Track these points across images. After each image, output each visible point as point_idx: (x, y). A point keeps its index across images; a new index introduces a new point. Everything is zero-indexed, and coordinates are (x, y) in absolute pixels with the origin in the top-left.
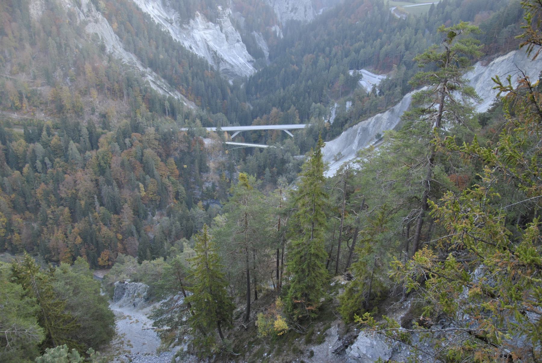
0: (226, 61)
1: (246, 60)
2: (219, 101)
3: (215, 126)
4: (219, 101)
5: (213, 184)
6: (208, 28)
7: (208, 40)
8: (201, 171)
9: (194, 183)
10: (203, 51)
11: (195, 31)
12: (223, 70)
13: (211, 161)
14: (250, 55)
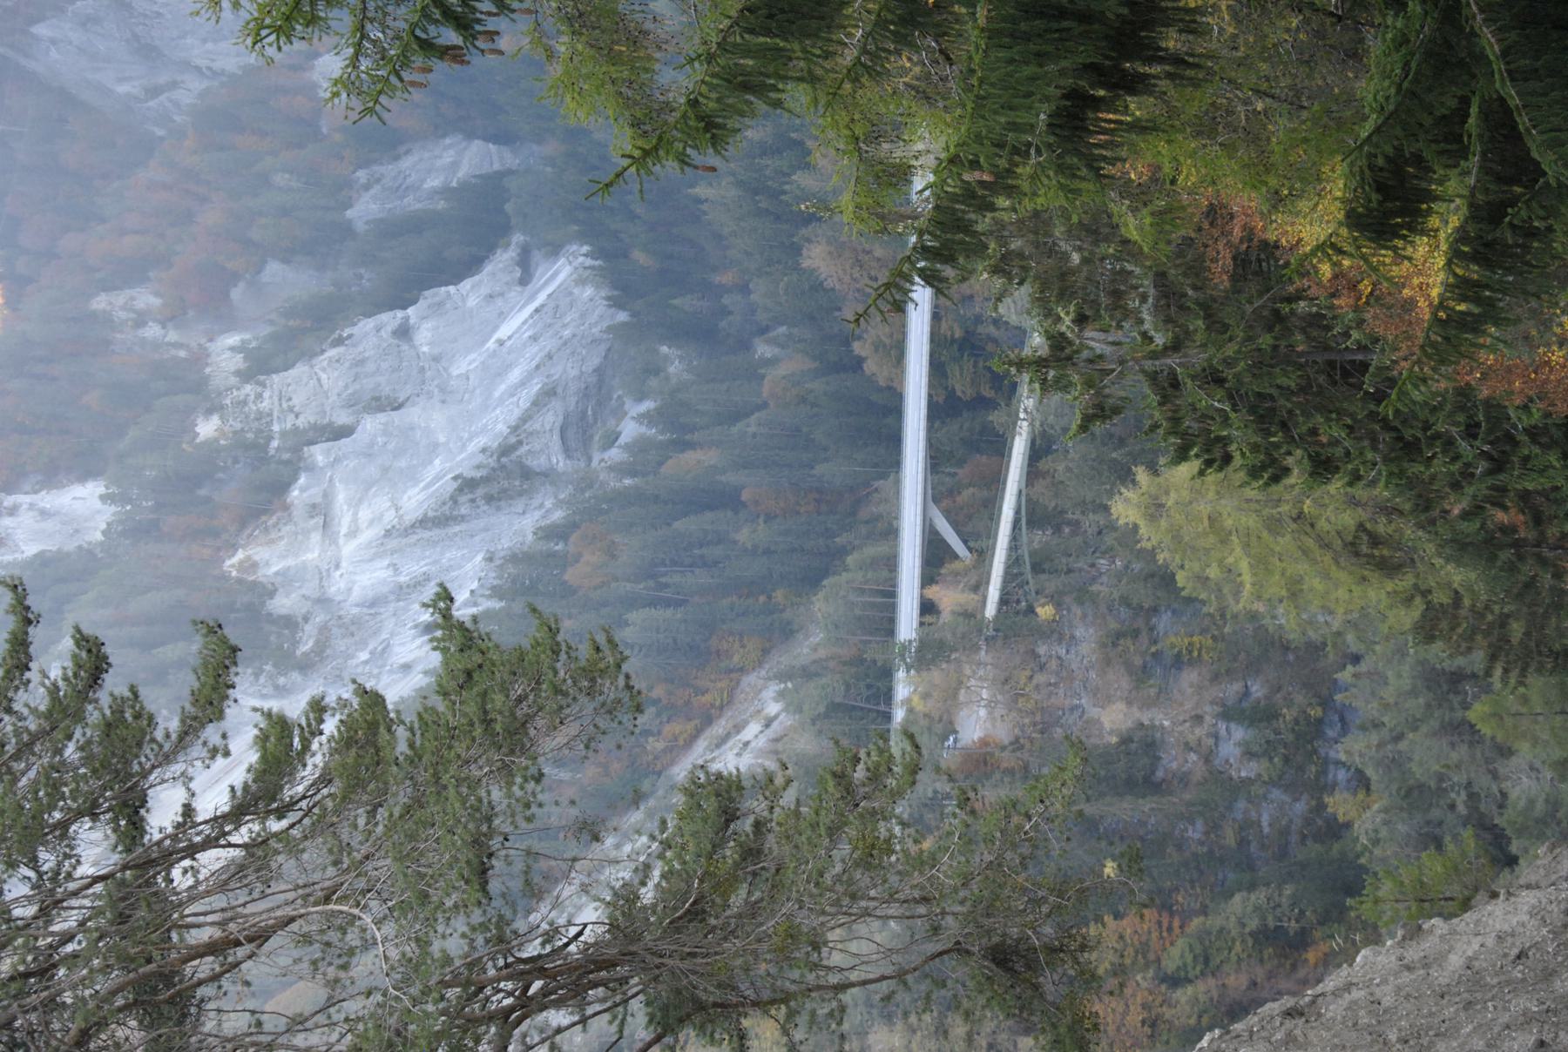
0: (515, 429)
1: (514, 293)
2: (744, 536)
3: (887, 674)
4: (744, 536)
5: (1228, 714)
6: (322, 512)
7: (390, 517)
8: (1148, 784)
9: (1214, 827)
10: (452, 554)
11: (336, 587)
12: (567, 451)
13: (1094, 712)
14: (488, 268)
